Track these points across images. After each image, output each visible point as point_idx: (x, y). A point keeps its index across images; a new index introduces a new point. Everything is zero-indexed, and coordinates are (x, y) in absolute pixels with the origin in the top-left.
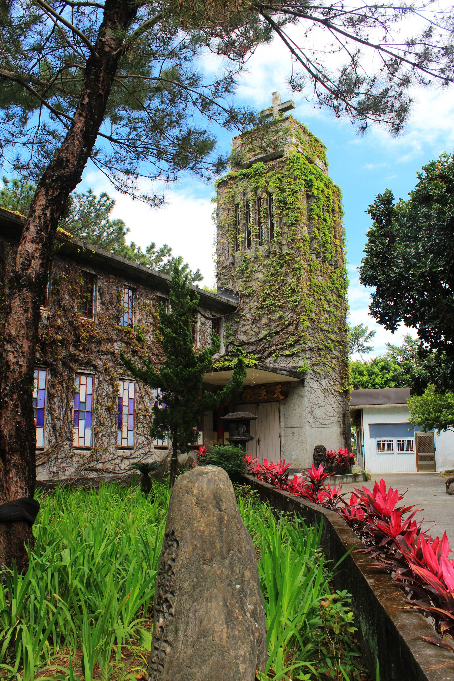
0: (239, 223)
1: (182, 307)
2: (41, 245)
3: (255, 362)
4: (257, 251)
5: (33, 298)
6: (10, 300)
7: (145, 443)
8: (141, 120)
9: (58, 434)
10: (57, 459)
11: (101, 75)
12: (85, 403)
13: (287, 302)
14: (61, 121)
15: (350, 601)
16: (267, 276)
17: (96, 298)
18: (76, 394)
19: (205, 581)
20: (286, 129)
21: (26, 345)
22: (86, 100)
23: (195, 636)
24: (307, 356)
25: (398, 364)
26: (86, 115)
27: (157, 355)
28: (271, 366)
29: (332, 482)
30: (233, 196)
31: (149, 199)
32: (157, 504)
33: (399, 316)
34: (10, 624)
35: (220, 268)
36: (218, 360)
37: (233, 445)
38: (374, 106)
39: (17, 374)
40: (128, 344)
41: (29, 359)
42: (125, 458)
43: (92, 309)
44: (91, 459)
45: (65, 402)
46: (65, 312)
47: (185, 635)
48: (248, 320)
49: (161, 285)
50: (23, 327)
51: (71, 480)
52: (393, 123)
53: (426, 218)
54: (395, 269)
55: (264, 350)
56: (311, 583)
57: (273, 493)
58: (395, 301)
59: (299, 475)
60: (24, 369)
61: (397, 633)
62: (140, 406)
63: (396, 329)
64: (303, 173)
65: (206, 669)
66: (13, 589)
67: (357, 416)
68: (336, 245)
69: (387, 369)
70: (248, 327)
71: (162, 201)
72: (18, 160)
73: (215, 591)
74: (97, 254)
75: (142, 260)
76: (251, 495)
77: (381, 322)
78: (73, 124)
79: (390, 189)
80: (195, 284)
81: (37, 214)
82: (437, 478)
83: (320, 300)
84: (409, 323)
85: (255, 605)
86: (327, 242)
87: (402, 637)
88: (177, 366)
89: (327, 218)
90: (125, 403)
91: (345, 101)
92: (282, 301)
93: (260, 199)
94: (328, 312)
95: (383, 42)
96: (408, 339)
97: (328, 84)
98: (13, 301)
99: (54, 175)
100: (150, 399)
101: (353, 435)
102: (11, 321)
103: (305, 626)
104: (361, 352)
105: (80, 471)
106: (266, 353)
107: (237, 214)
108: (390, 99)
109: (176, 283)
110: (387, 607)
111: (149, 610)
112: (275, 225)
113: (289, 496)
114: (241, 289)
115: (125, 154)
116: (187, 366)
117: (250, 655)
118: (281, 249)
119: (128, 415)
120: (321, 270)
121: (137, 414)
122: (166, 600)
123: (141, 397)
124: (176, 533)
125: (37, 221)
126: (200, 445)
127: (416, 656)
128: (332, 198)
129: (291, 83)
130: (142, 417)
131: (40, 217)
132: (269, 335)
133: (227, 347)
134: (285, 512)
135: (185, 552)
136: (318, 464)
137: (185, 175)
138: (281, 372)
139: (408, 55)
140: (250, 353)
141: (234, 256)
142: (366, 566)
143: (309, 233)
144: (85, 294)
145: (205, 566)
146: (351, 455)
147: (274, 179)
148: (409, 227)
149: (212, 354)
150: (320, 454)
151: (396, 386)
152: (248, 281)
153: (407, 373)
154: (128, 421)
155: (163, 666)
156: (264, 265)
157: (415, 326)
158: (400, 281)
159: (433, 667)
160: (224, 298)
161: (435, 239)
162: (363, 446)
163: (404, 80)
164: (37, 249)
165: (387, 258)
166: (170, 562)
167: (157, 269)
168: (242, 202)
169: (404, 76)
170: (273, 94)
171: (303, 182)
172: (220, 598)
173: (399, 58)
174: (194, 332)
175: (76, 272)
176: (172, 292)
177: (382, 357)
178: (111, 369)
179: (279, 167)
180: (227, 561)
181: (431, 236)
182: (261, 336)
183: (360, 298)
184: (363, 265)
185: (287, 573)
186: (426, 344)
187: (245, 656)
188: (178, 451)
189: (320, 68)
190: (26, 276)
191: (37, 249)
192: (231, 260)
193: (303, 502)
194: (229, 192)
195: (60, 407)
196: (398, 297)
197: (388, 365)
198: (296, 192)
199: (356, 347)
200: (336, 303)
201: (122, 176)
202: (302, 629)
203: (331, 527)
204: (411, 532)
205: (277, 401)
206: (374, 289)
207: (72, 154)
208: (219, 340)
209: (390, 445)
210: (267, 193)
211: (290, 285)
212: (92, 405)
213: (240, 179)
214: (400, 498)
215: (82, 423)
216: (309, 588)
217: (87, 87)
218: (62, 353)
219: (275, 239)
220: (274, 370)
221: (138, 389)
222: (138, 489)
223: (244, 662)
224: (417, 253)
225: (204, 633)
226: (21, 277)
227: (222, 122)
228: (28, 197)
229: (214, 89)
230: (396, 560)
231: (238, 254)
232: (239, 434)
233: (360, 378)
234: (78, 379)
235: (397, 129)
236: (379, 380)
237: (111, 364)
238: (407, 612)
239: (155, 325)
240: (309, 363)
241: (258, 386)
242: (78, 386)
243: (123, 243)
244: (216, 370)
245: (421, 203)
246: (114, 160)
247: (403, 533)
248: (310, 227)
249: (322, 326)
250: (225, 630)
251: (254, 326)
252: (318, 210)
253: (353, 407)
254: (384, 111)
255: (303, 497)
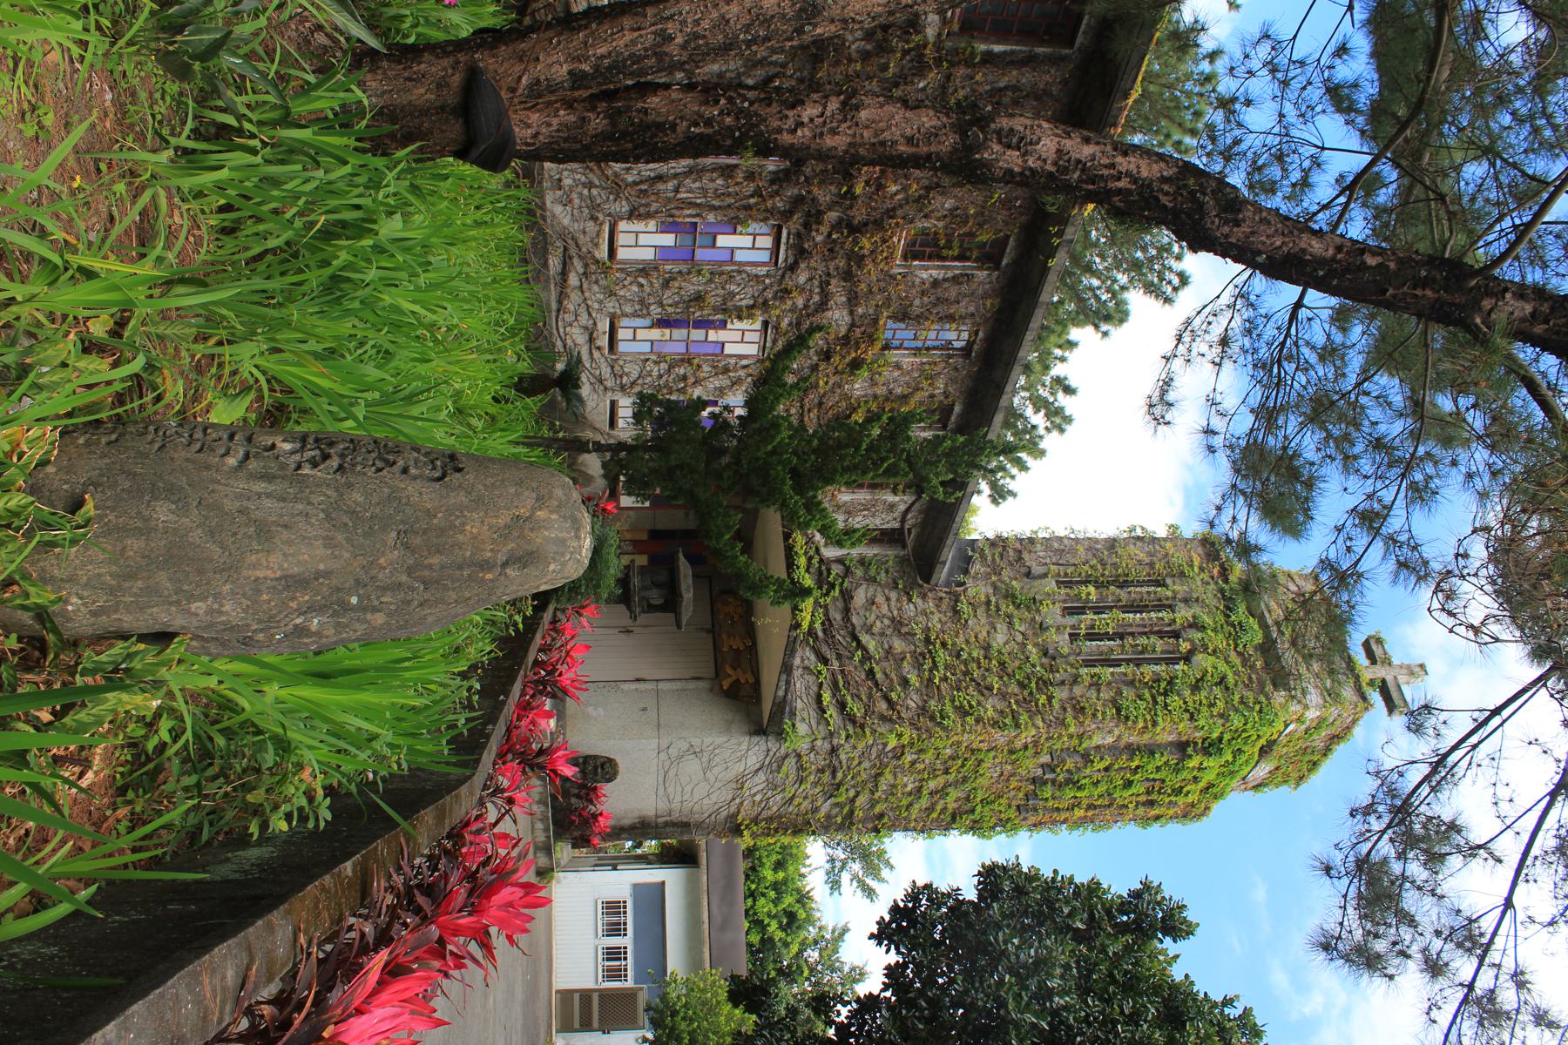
0: (1121, 587)
1: (927, 462)
2: (1053, 169)
3: (805, 625)
4: (1058, 629)
5: (937, 154)
6: (934, 107)
7: (625, 379)
8: (1340, 375)
9: (643, 187)
10: (590, 185)
11: (1429, 293)
12: (714, 246)
13: (941, 698)
14: (1337, 197)
15: (311, 825)
16: (999, 652)
17: (948, 268)
18: (733, 227)
19: (366, 535)
20: (1338, 695)
21: (837, 142)
22: (1371, 261)
23: (258, 515)
24: (819, 743)
25: (801, 952)
26: (1339, 262)
27: (820, 404)
28: (797, 661)
29: (537, 798)
30: (1182, 574)
31: (1163, 392)
32: (493, 410)
33: (910, 951)
34: (260, 123)
35: (1018, 546)
36: (810, 541)
37: (620, 575)
38: (1377, 894)
39: (776, 124)
40: (846, 340)
41: (808, 148)
42: (591, 334)
43: (922, 259)
44: (589, 260)
45: (716, 203)
46: (917, 201)
47: (259, 495)
48: (900, 609)
49: (980, 415)
50: (876, 135)
51: (544, 218)
52: (1339, 937)
53: (1131, 1014)
54: (1016, 941)
55: (833, 645)
56: (343, 744)
57: (518, 663)
58: (942, 942)
59: (552, 723)
60: (786, 138)
61: (260, 916)
62: (706, 368)
63: (880, 944)
64: (1237, 734)
65: (196, 536)
66: (332, 127)
67: (682, 856)
68: (1072, 808)
69: (789, 924)
70: (885, 609)
71: (1160, 421)
72: (1248, 103)
73: (347, 555)
74: (1045, 270)
75: (1038, 367)
76: (511, 616)
77: (895, 909)
78: (1319, 233)
79: (1198, 931)
80: (984, 486)
81: (1119, 159)
82: (543, 1035)
83: (946, 772)
84: (891, 971)
85: (318, 634)
86: (1079, 788)
87: (252, 924)
88: (795, 453)
89: (1134, 790)
90: (713, 335)
91: (1389, 826)
92: (944, 686)
93: (1176, 635)
94: (919, 789)
95: (1521, 916)
96: (859, 975)
97: (1425, 790)
98: (931, 113)
99: (1204, 194)
100: (721, 391)
101: (639, 845)
102: (889, 108)
103: (259, 732)
104: (828, 866)
105: (563, 235)
106: (825, 649)
107: (1141, 584)
108: (1393, 930)
109: (982, 449)
110: (302, 900)
111: (282, 405)
112: (1118, 670)
113: (510, 701)
114: (971, 592)
115: (1265, 337)
116: (795, 473)
117: (223, 623)
118: (1063, 683)
119: (687, 341)
120: (1013, 775)
121: (689, 362)
122: (326, 457)
123: (726, 370)
124: (458, 475)
125: (1105, 161)
126: (618, 501)
127: (219, 951)
128: (1181, 800)
129: (1426, 707)
130: (682, 371)
131: (1112, 166)
132: (867, 657)
133: (840, 561)
134: (479, 692)
135: (420, 493)
136: (576, 765)
137: (1220, 473)
138: (782, 683)
139: (1492, 972)
140: (826, 614)
141: (1045, 575)
142: (376, 861)
143: (1098, 747)
144: (956, 243)
145: (394, 534)
146: (596, 840)
147: (1222, 667)
148: (1111, 975)
149: (823, 530)
150: (599, 769)
151: (750, 945)
152: (988, 609)
153: (780, 972)
154: (674, 341)
155: (200, 451)
156: (1024, 645)
157: (886, 987)
158: (989, 954)
159: (206, 981)
160: (949, 555)
161: (1083, 1034)
162: (615, 869)
163: (1436, 964)
164: (1045, 161)
165: (1041, 924)
166: (401, 463)
167: (1016, 401)
168: (1169, 594)
169: (1447, 964)
170: (1422, 666)
171: (1215, 735)
172: (333, 565)
173: (1486, 952)
174: (873, 487)
175: (1006, 223)
176: (962, 439)
177: (818, 915)
178: (789, 303)
179: (1250, 678)
180: (404, 578)
181: (1089, 1025)
182: (865, 638)
183: (949, 862)
184: (1025, 870)
185: (368, 697)
186: (844, 1011)
187: (221, 613)
188: (608, 455)
189: (1460, 770)
190: (986, 139)
191: (1045, 161)
192: (1037, 570)
193: (500, 729)
194: (1192, 566)
195: (704, 191)
196: (951, 948)
197: (799, 928)
198: (1192, 718)
199: (840, 854)
200: (939, 808)
201: (1217, 330)
202: (254, 725)
203: (449, 792)
204: (444, 958)
205: (718, 673)
206: (970, 894)
207: (1252, 233)
208: (853, 544)
209: (615, 929)
210: (1191, 652)
211: (979, 703)
212: (709, 262)
213: (1222, 591)
214: (509, 938)
215: (668, 240)
216: (333, 740)
217: (1400, 261)
218: (823, 195)
219: (1084, 671)
220: (787, 669)
221: (745, 362)
222: (525, 367)
223: (210, 612)
224: (1050, 993)
225: (264, 532)
226: (982, 129)
227: (1332, 555)
228: (1177, 108)
229: (1403, 538)
230: (390, 925)
231: (1050, 585)
232: (644, 588)
233: (769, 863)
234: (765, 229)
235: (1326, 947)
236: (764, 906)
237: (800, 302)
238: (296, 939)
239: (887, 399)
240: (803, 746)
241: (751, 632)
242: (750, 230)
243: (1078, 324)
244: (787, 536)
245: (1166, 1002)
246: (1251, 313)
247: (441, 941)
248: (1114, 750)
249: (888, 776)
250: (269, 573)
251: (887, 622)
252: (1150, 767)
253: (703, 847)
254: (1366, 916)
255: (509, 731)
